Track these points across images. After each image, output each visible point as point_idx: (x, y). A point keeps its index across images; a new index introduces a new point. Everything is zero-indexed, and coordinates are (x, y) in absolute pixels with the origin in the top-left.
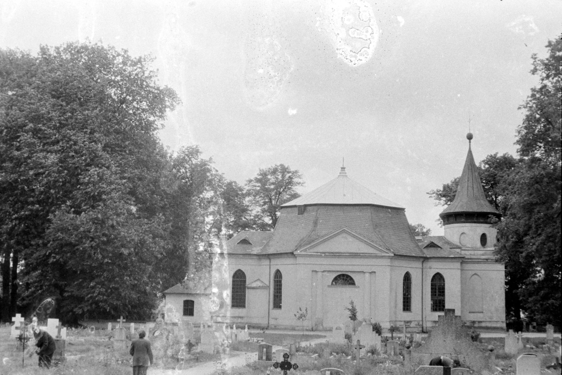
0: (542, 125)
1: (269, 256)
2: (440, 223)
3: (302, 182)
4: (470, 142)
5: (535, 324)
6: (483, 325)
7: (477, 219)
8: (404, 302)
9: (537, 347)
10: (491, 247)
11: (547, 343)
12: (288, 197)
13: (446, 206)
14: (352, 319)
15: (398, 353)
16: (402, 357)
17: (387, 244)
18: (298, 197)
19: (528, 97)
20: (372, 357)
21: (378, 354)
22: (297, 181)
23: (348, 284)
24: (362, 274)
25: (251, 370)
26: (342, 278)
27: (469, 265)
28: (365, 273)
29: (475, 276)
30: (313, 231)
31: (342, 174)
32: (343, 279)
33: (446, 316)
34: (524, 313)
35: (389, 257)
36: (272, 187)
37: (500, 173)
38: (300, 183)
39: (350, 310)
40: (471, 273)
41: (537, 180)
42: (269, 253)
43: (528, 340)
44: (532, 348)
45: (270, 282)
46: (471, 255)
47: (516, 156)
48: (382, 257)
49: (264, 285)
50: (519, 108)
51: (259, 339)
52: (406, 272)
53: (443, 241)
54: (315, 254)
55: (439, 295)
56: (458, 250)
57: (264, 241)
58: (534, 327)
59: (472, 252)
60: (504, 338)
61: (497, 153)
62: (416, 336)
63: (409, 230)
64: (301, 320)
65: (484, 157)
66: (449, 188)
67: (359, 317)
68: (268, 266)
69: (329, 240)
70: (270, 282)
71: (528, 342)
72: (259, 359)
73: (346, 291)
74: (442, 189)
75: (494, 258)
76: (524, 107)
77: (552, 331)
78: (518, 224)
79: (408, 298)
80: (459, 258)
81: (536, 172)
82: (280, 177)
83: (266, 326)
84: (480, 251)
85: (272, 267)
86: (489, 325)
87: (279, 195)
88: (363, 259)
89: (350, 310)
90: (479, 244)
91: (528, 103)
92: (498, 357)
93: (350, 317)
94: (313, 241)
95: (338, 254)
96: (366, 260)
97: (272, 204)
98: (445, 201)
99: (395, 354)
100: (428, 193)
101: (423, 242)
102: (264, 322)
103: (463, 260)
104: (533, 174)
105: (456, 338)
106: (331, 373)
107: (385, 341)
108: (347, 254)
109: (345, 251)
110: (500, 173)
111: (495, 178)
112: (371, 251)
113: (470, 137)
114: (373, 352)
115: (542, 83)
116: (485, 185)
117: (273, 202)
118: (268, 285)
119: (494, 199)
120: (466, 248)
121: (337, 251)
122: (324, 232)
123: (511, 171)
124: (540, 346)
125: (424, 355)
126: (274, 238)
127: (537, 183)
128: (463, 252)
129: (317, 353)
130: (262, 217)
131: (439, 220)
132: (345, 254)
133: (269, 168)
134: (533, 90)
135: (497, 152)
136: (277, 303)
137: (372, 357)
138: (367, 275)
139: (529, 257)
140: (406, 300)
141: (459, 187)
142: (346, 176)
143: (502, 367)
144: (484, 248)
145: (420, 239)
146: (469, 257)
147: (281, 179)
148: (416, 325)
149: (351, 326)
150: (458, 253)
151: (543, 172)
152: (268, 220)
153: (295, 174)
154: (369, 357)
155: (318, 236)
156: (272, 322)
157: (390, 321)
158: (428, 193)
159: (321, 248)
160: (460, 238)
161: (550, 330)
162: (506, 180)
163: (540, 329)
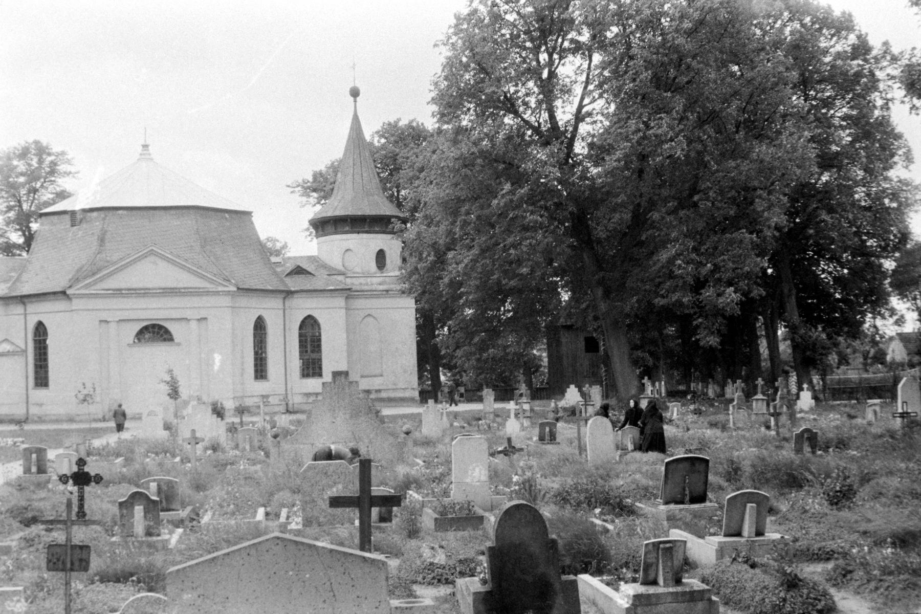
0: (472, 73)
1: (23, 299)
2: (309, 235)
3: (73, 170)
4: (355, 101)
5: (462, 390)
6: (384, 395)
7: (370, 226)
8: (256, 365)
9: (469, 424)
10: (393, 270)
11: (485, 418)
12: (51, 196)
13: (318, 207)
14: (171, 398)
15: (257, 447)
16: (262, 453)
17: (224, 272)
18: (68, 197)
19: (450, 27)
20: (214, 457)
21: (224, 451)
22: (64, 170)
23: (161, 341)
24: (184, 323)
25: (15, 492)
26: (151, 330)
27: (357, 300)
28: (189, 320)
29: (370, 319)
30: (98, 253)
31: (143, 157)
32: (154, 333)
33: (335, 382)
34: (445, 375)
35: (228, 293)
36: (22, 179)
37: (403, 153)
38: (70, 173)
39: (168, 383)
40: (362, 314)
41: (467, 163)
42: (24, 293)
43: (456, 415)
44: (464, 427)
45: (26, 343)
46: (361, 284)
47: (430, 124)
48: (217, 293)
49: (19, 350)
50: (436, 45)
51: (16, 440)
52: (257, 316)
53: (316, 264)
54: (103, 292)
55: (312, 352)
56: (340, 278)
57: (13, 274)
58: (462, 395)
59: (362, 280)
60: (419, 414)
61: (399, 120)
62: (281, 419)
63: (260, 247)
64: (86, 403)
65: (378, 127)
66: (322, 176)
67: (184, 392)
68: (23, 317)
69: (131, 265)
70: (26, 343)
71: (456, 418)
72: (25, 473)
73: (157, 352)
74: (311, 179)
75: (399, 288)
76: (444, 45)
77: (492, 398)
78: (436, 233)
79: (261, 359)
80: (342, 290)
81: (465, 148)
82: (35, 163)
83: (23, 418)
84: (376, 279)
85: (28, 317)
86: (392, 395)
87: (35, 194)
88: (189, 298)
89: (168, 383)
90: (373, 266)
91: (449, 38)
92: (416, 443)
93: (169, 395)
94: (99, 270)
95: (143, 292)
96: (177, 299)
97: (22, 210)
98: (317, 198)
99: (252, 448)
100: (288, 186)
101: (282, 266)
102: (19, 411)
103: (348, 293)
104: (459, 152)
105: (351, 417)
106: (158, 485)
107: (232, 429)
108: (158, 291)
109: (156, 286)
110: (403, 153)
111: (396, 160)
112: (195, 282)
113: (355, 93)
114: (215, 448)
115: (470, 6)
116: (380, 171)
117: (25, 207)
118: (23, 347)
119: (396, 194)
120: (354, 273)
121: (141, 286)
122: (115, 257)
123: (420, 148)
124: (474, 423)
125: (302, 446)
126: (30, 268)
127: (466, 166)
128: (349, 281)
129: (121, 456)
130: (6, 232)
131: (308, 229)
132: (154, 291)
133: (15, 148)
134: (458, 17)
135: (398, 117)
136: (42, 379)
137: (214, 457)
138: (194, 324)
139: (455, 285)
140: (259, 362)
141: (339, 175)
142: (152, 159)
143: (424, 459)
144: (382, 273)
145: (279, 261)
146: (358, 288)
147: (36, 165)
148: (280, 400)
149: (172, 410)
150: (341, 282)
151: (474, 150)
152: (16, 238)
153: (60, 157)
154: (209, 456)
155: (108, 262)
156: (34, 410)
157: (234, 398)
158: (288, 186)
159: (114, 283)
160: (343, 259)
161: (488, 397)
162: (415, 163)
163: (473, 395)
